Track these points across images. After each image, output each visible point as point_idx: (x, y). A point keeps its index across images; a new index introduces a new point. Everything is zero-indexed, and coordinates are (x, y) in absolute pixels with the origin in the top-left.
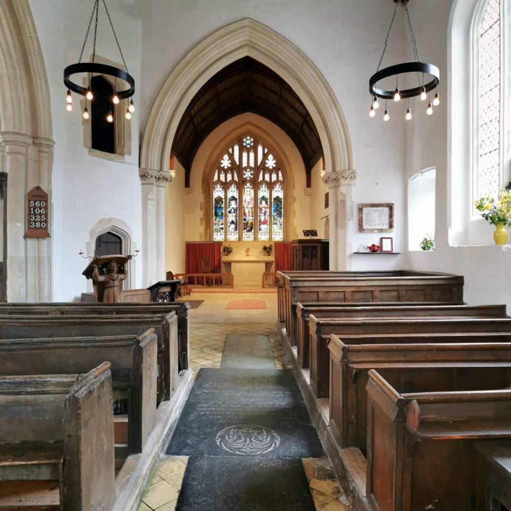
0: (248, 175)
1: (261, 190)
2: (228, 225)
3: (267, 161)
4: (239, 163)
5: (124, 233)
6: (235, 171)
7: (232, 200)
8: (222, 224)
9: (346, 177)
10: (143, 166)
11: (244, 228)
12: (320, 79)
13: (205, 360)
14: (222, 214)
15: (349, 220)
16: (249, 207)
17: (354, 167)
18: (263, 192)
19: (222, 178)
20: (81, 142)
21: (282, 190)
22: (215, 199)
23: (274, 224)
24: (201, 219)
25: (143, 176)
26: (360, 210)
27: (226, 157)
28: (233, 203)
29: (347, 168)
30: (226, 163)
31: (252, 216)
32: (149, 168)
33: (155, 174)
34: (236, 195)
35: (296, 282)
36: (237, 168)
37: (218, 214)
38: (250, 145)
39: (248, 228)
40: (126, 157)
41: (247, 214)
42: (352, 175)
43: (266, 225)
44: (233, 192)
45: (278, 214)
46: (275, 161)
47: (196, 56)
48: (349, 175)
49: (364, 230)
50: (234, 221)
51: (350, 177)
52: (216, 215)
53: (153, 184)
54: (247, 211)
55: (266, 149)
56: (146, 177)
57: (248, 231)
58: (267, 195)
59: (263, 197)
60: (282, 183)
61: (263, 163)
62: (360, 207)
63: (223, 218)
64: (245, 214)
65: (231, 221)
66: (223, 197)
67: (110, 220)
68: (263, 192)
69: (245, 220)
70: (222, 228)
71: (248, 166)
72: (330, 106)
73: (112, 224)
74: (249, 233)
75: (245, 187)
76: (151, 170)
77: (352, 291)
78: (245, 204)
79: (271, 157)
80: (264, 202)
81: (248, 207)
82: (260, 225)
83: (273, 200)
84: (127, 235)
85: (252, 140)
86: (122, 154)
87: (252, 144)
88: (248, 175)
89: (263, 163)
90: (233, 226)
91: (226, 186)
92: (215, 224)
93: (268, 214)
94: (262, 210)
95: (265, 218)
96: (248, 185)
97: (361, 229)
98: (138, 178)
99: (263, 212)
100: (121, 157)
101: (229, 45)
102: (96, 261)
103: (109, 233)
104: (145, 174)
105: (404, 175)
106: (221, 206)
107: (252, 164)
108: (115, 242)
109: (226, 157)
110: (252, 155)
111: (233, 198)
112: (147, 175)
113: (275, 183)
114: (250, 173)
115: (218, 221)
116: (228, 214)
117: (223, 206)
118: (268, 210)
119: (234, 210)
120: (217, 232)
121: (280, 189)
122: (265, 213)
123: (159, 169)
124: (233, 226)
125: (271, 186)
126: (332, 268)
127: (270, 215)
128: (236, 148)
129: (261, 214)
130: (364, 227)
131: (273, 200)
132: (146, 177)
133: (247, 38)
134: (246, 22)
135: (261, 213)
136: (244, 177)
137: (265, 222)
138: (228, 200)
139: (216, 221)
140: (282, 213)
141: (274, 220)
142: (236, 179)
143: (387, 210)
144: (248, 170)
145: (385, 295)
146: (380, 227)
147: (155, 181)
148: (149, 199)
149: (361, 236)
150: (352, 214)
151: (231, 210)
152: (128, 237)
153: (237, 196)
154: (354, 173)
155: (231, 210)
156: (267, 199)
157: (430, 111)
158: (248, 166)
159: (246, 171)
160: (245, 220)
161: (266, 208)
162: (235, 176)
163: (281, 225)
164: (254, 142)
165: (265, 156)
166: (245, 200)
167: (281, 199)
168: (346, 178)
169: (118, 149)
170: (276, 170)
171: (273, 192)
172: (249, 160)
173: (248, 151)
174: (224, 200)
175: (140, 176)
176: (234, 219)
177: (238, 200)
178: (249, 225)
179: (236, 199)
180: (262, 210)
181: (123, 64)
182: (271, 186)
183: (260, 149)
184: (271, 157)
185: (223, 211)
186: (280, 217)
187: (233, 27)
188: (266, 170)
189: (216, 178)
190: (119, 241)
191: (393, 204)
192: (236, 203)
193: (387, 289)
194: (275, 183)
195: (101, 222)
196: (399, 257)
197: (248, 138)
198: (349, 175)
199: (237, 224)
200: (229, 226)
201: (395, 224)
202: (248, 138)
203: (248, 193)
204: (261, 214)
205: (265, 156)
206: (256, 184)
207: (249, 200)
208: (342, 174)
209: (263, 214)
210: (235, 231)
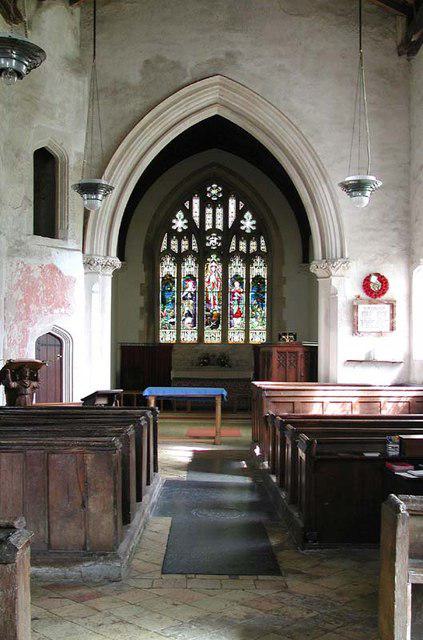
0: (213, 241)
8: (173, 317)
10: (87, 251)
18: (237, 268)
19: (174, 247)
24: (141, 308)
27: (180, 214)
28: (190, 284)
29: (339, 256)
30: (180, 224)
36: (196, 231)
41: (212, 302)
43: (240, 319)
44: (190, 267)
52: (164, 302)
54: (211, 296)
57: (212, 328)
58: (242, 272)
61: (237, 223)
64: (208, 301)
68: (237, 268)
69: (208, 310)
70: (173, 323)
71: (214, 229)
74: (214, 331)
79: (248, 215)
80: (237, 284)
81: (213, 294)
88: (213, 241)
89: (237, 223)
91: (179, 259)
93: (243, 302)
96: (214, 257)
97: (355, 330)
99: (236, 298)
107: (220, 227)
109: (180, 214)
110: (219, 211)
111: (191, 277)
117: (175, 289)
118: (243, 295)
125: (248, 259)
127: (247, 304)
128: (196, 202)
142: (195, 248)
143: (388, 307)
158: (214, 229)
160: (208, 310)
161: (240, 293)
165: (240, 215)
169: (60, 233)
172: (214, 219)
183: (232, 203)
184: (248, 215)
192: (195, 284)
194: (254, 255)
201: (397, 325)
206: (226, 258)
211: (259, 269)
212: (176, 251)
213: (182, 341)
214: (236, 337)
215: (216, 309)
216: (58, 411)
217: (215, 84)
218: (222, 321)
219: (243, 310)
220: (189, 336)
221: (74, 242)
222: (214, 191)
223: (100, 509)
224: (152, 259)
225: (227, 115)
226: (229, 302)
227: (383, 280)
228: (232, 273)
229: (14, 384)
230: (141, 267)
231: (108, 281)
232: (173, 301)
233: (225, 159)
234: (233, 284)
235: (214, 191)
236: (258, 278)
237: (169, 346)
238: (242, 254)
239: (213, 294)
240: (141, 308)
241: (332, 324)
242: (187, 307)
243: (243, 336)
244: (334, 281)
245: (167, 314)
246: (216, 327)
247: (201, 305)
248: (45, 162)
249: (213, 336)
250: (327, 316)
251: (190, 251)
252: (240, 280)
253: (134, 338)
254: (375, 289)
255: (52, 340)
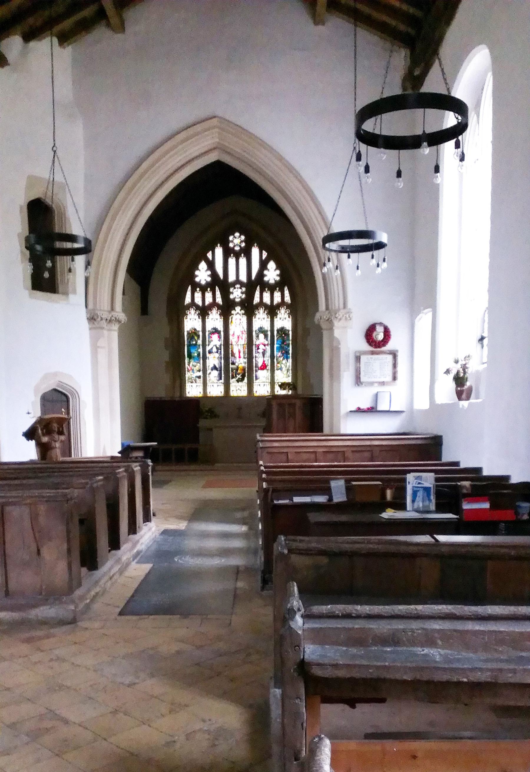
0: (237, 294)
1: (257, 316)
2: (208, 372)
3: (265, 272)
4: (224, 277)
5: (72, 389)
6: (217, 288)
7: (213, 333)
8: (199, 371)
9: (339, 317)
10: (90, 306)
11: (232, 375)
12: (309, 194)
13: (104, 191)
14: (199, 355)
15: (345, 371)
16: (239, 343)
17: (350, 305)
18: (261, 320)
19: (198, 300)
20: (21, 284)
21: (289, 317)
22: (188, 333)
23: (277, 370)
24: (166, 362)
25: (92, 319)
26: (358, 359)
27: (203, 265)
28: (215, 337)
29: (342, 306)
30: (202, 275)
31: (244, 358)
32: (98, 308)
33: (106, 316)
34: (220, 326)
35: (264, 443)
36: (220, 283)
37: (192, 355)
38: (240, 246)
39: (239, 376)
40: (71, 296)
41: (237, 355)
42: (347, 316)
43: (265, 371)
44: (215, 320)
45: (283, 354)
46: (278, 272)
47: (153, 165)
48: (343, 316)
49: (362, 383)
50: (217, 366)
51: (344, 318)
52: (190, 356)
53: (102, 328)
54: (236, 351)
55: (264, 252)
56: (95, 320)
57: (238, 381)
58: (267, 325)
59: (261, 328)
60: (288, 306)
61: (261, 275)
62: (358, 355)
63: (200, 361)
64: (233, 355)
65: (212, 366)
66: (199, 328)
67: (55, 374)
68: (261, 320)
69: (233, 363)
70: (199, 377)
71: (237, 281)
72: (321, 228)
73: (58, 379)
74: (240, 383)
75: (233, 312)
76: (101, 310)
77: (324, 452)
78: (233, 339)
79: (272, 265)
80: (261, 336)
81: (238, 344)
82: (256, 371)
83: (275, 333)
84: (75, 392)
85: (243, 237)
86: (66, 293)
87: (243, 245)
88: (237, 294)
89: (261, 275)
90: (215, 373)
91: (204, 312)
92: (189, 371)
93: (268, 353)
94: (258, 349)
95: (264, 361)
96: (238, 309)
97: (358, 381)
98: (86, 321)
99: (261, 351)
100: (64, 297)
101: (194, 150)
102: (40, 421)
103: (55, 390)
104: (93, 316)
105: (412, 316)
106: (196, 342)
107: (243, 278)
108: (61, 401)
109: (203, 265)
110: (243, 261)
111: (216, 331)
112: (95, 317)
113: (279, 306)
114: (240, 290)
115: (193, 365)
116: (208, 355)
117: (200, 342)
118: (268, 348)
119: (217, 348)
120: (192, 382)
121: (286, 316)
122: (264, 354)
123: (109, 308)
124: (215, 373)
125: (272, 311)
126: (326, 429)
127: (272, 356)
128: (219, 251)
129: (257, 355)
130: (362, 380)
131: (275, 333)
132: (95, 320)
133: (217, 140)
134: (215, 121)
135: (258, 352)
136: (232, 297)
137: (264, 367)
138: (207, 333)
139: (189, 365)
140: (290, 352)
141: (278, 363)
142: (219, 300)
143: (390, 358)
144: (238, 286)
145: (358, 455)
146: (382, 380)
147: (106, 324)
148: (99, 347)
149: (360, 390)
150: (348, 363)
151: (212, 349)
152: (76, 395)
153: (221, 328)
154: (349, 312)
155: (212, 349)
156: (267, 331)
157: (379, 270)
158: (237, 281)
159: (235, 288)
160: (233, 363)
161: (265, 345)
162: (217, 296)
163: (288, 370)
164: (245, 241)
165: (263, 265)
166: (234, 334)
167: (289, 331)
168: (340, 319)
169: (61, 288)
170: (279, 285)
171: (275, 319)
172: (238, 270)
173: (237, 256)
174: (201, 334)
175: (88, 319)
176: (216, 363)
177: (222, 333)
178: (239, 371)
179: (218, 332)
180: (258, 349)
181: (64, 181)
182: (272, 311)
183: (255, 251)
184: (272, 265)
185: (201, 350)
186: (287, 358)
187: (198, 128)
188: (264, 286)
189: (188, 300)
190: (66, 399)
191: (397, 351)
192: (219, 337)
193: (359, 449)
194: (279, 306)
195: (46, 377)
196: (404, 415)
197: (237, 234)
198: (343, 316)
199: (221, 370)
200: (210, 373)
201: (399, 375)
202: (237, 234)
203: (238, 321)
204: (257, 355)
205: (263, 265)
206: (250, 309)
207: (240, 334)
208: (336, 314)
209: (261, 355)
210: (218, 380)
211: (284, 321)
212: (200, 304)
213: (209, 395)
214: (262, 389)
215: (241, 362)
216: (16, 466)
217: (214, 127)
218: (248, 374)
219: (268, 362)
220: (216, 390)
221: (77, 298)
222: (237, 241)
223: (56, 560)
224: (177, 311)
225: (227, 160)
226: (254, 355)
227: (387, 333)
228: (256, 326)
229: (45, 439)
230: (165, 320)
231: (115, 335)
232: (199, 355)
233: (218, 204)
234: (258, 336)
235: (237, 241)
236: (282, 331)
237: (195, 401)
238: (266, 306)
239: (238, 344)
240: (166, 362)
241: (335, 376)
242: (213, 360)
243: (201, 389)
244: (337, 333)
245: (192, 369)
246: (242, 380)
247: (226, 358)
248: (40, 214)
249: (239, 390)
250: (331, 368)
251: (214, 304)
252: (265, 332)
253: (160, 392)
254: (376, 339)
255: (56, 396)
